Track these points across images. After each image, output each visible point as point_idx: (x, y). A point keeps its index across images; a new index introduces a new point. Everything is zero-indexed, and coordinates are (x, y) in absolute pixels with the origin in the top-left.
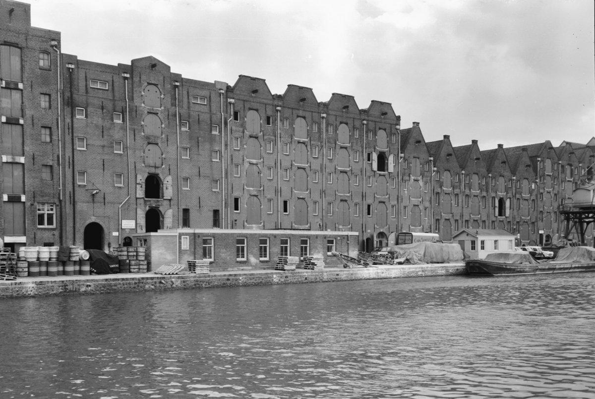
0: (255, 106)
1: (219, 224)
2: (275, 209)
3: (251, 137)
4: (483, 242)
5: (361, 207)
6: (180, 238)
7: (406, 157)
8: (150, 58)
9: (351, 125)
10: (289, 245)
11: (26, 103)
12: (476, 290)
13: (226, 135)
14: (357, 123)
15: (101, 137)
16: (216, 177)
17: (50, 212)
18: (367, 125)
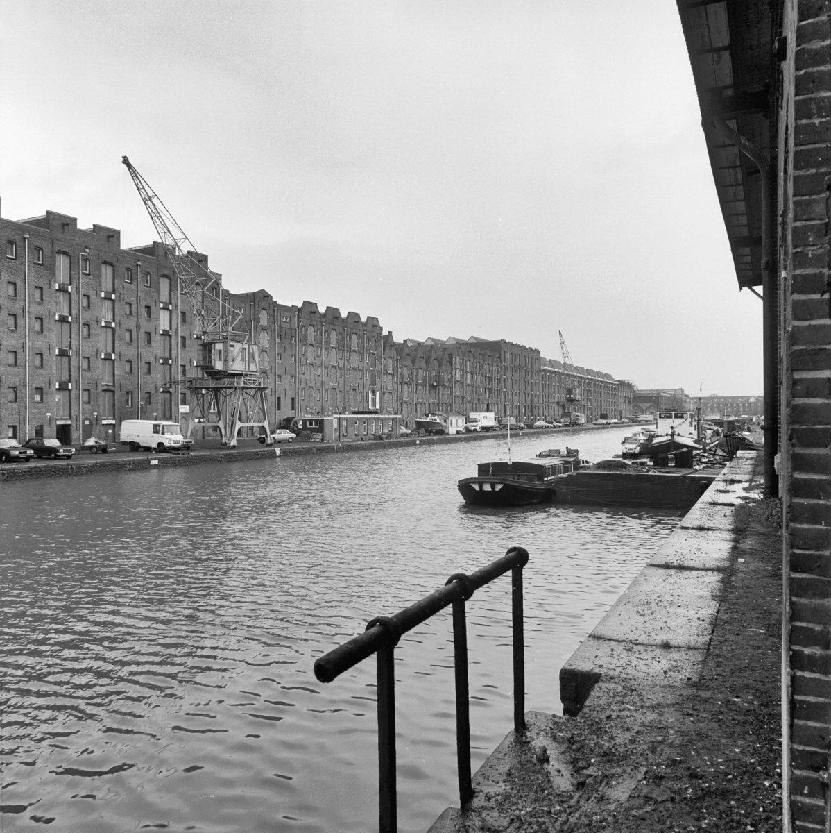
8: (262, 291)
16: (294, 373)
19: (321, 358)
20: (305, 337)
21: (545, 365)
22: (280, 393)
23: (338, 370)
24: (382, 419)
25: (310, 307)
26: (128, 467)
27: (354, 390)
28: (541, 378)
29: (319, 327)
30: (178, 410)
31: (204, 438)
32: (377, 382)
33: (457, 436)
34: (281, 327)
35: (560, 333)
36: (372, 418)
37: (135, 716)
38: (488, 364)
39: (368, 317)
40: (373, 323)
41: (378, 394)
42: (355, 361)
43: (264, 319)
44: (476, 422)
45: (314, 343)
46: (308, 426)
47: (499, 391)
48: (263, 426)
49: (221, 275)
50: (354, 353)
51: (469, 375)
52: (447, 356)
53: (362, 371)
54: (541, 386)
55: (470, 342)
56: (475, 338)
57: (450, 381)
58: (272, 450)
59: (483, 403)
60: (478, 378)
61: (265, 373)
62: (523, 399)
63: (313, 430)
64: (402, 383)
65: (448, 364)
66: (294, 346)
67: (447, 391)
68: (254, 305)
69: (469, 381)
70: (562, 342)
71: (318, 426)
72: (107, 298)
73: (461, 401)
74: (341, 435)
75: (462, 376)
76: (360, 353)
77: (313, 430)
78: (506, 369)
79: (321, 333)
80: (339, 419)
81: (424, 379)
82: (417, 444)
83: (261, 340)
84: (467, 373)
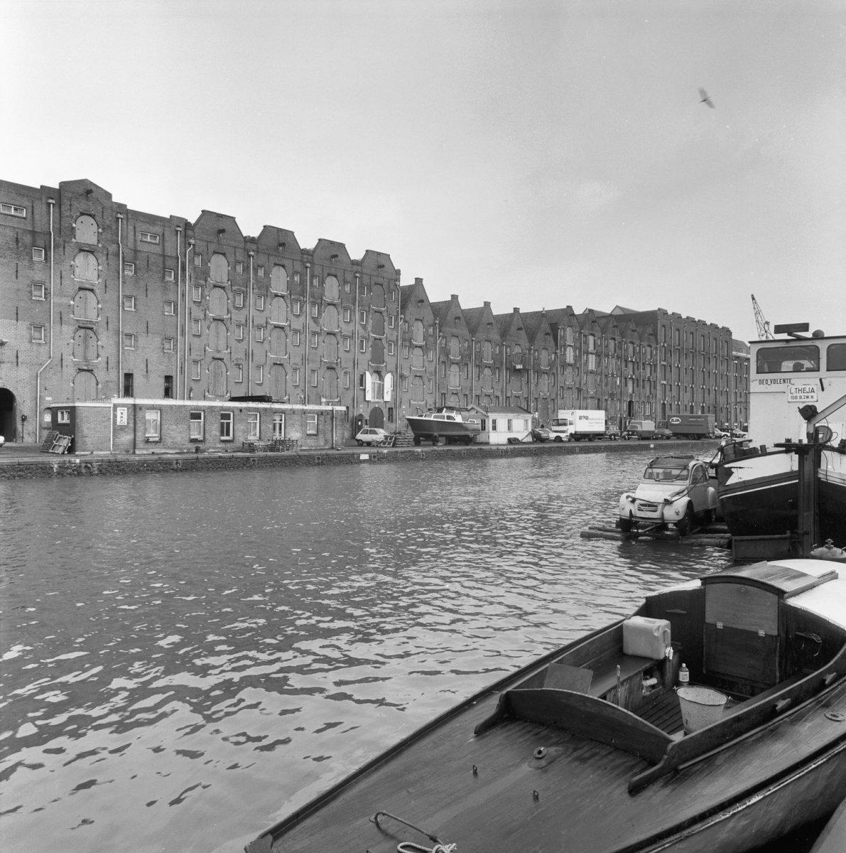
0: (333, 271)
2: (245, 376)
4: (494, 422)
7: (408, 319)
9: (341, 278)
10: (232, 420)
13: (184, 281)
14: (349, 277)
15: (14, 277)
16: (170, 333)
20: (205, 274)
21: (740, 350)
24: (283, 412)
28: (732, 368)
29: (240, 257)
32: (386, 358)
34: (136, 251)
35: (753, 299)
36: (249, 409)
37: (293, 711)
38: (650, 346)
39: (367, 251)
41: (388, 379)
42: (331, 319)
43: (87, 232)
44: (565, 425)
45: (227, 284)
47: (653, 385)
53: (352, 337)
54: (733, 379)
55: (615, 313)
57: (551, 364)
59: (620, 400)
60: (612, 364)
61: (91, 329)
62: (699, 397)
64: (446, 362)
65: (550, 338)
66: (172, 287)
67: (545, 380)
73: (575, 395)
76: (346, 309)
78: (668, 351)
80: (135, 408)
81: (497, 359)
82: (651, 449)
83: (77, 271)
84: (588, 353)
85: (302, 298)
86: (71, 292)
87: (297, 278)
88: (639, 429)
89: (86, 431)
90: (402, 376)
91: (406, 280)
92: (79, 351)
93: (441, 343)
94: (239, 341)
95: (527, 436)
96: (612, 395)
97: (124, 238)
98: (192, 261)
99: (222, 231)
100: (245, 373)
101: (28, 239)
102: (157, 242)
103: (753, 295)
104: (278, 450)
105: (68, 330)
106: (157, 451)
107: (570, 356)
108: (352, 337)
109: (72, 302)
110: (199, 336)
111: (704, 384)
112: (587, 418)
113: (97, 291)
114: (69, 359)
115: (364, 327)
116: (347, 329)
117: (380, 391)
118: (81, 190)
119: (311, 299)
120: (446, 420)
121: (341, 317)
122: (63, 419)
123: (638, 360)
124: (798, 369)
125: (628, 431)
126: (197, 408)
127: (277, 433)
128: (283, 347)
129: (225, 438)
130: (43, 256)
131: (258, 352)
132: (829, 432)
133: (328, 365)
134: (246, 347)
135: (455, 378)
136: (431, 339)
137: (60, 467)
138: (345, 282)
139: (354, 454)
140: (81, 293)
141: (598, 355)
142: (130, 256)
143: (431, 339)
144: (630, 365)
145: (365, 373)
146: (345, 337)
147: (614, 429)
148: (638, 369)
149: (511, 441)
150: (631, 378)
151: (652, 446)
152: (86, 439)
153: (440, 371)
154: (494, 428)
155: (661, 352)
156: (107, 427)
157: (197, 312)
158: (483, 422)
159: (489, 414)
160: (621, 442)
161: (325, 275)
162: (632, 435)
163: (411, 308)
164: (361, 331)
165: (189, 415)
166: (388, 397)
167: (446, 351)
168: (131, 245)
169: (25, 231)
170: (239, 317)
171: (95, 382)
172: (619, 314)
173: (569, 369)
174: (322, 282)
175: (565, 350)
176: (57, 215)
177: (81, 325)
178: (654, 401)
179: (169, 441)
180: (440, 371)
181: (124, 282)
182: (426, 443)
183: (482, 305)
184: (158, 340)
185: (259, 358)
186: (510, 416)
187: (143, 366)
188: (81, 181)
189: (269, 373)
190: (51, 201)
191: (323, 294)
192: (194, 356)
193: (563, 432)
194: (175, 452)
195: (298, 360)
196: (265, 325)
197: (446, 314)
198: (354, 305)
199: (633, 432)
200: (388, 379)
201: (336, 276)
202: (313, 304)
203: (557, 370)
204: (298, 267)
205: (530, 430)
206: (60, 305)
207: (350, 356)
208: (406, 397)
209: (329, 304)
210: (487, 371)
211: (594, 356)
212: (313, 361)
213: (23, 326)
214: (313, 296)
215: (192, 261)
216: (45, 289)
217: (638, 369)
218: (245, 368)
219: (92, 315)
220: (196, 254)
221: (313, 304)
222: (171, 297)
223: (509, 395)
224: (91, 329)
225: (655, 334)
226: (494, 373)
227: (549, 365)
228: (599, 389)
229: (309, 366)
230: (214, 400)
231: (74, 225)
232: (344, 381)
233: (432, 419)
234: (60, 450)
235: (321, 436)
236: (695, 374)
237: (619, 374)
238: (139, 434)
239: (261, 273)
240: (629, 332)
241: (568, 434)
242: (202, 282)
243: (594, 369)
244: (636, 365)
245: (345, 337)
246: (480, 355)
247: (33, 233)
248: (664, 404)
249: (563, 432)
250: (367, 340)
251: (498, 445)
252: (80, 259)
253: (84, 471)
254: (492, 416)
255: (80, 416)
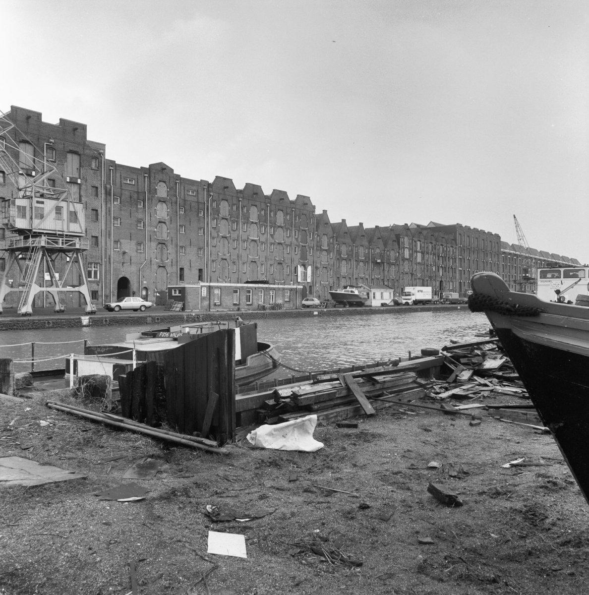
0: (281, 208)
1: (202, 279)
2: (237, 268)
3: (223, 219)
4: (374, 294)
5: (291, 268)
6: (201, 289)
7: (319, 234)
8: (161, 164)
9: (285, 211)
10: (238, 294)
11: (82, 193)
12: (294, 343)
13: (208, 216)
14: (289, 211)
15: (129, 217)
16: (201, 245)
17: (96, 269)
18: (270, 206)
19: (265, 235)
20: (217, 211)
22: (184, 263)
23: (259, 244)
24: (274, 289)
25: (223, 185)
26: (48, 326)
27: (280, 264)
28: (501, 260)
29: (235, 202)
30: (43, 277)
31: (80, 306)
33: (382, 308)
34: (185, 200)
35: (515, 217)
36: (259, 288)
38: (452, 247)
39: (298, 195)
40: (304, 202)
41: (309, 269)
42: (280, 235)
43: (162, 191)
44: (410, 295)
46: (173, 294)
48: (80, 292)
49: (104, 145)
50: (280, 229)
51: (419, 255)
52: (394, 236)
54: (501, 266)
56: (434, 223)
57: (397, 259)
58: (77, 319)
60: (430, 258)
61: (164, 244)
63: (176, 298)
64: (340, 259)
65: (396, 244)
67: (393, 268)
68: (149, 177)
69: (419, 260)
70: (517, 226)
71: (180, 295)
72: (73, 182)
74: (212, 304)
75: (411, 255)
76: (287, 229)
77: (176, 298)
78: (463, 250)
79: (238, 208)
80: (210, 288)
83: (158, 212)
84: (417, 252)
85: (265, 223)
86: (155, 223)
87: (263, 212)
88: (450, 297)
89: (189, 300)
90: (317, 268)
91: (318, 211)
92: (159, 256)
93: (337, 248)
94: (234, 249)
95: (391, 302)
96: (430, 277)
97: (180, 193)
98: (212, 205)
99: (227, 187)
100: (237, 266)
101: (135, 196)
102: (195, 195)
103: (514, 215)
104: (275, 310)
105: (154, 244)
106: (219, 310)
107: (407, 254)
108: (291, 245)
109: (156, 230)
110: (215, 246)
111: (478, 269)
112: (422, 291)
113: (167, 223)
114: (155, 261)
115: (297, 239)
116: (288, 241)
117: (305, 275)
118: (159, 168)
119: (270, 224)
120: (350, 293)
121: (285, 234)
122: (175, 293)
123: (445, 256)
124: (553, 277)
125: (444, 299)
126: (236, 287)
127: (271, 301)
128: (256, 252)
129: (248, 303)
130: (142, 205)
131: (244, 254)
132: (564, 298)
133: (278, 262)
134: (266, 255)
135: (344, 269)
136: (331, 245)
137: (187, 317)
138: (287, 214)
139: (311, 311)
140: (160, 224)
141: (423, 253)
142: (182, 204)
143: (331, 245)
144: (441, 259)
145: (297, 266)
146: (287, 246)
147: (436, 298)
148: (445, 260)
149: (383, 305)
150: (442, 267)
151: (459, 308)
152: (189, 304)
153: (336, 264)
154: (374, 297)
155: (458, 250)
156: (198, 297)
157: (215, 234)
158: (368, 294)
159: (371, 290)
160: (440, 306)
161: (277, 210)
162: (446, 301)
163: (321, 228)
164: (295, 242)
165: (232, 291)
166: (309, 280)
167: (339, 253)
168: (182, 197)
169: (135, 192)
170: (234, 235)
171: (166, 273)
172: (433, 226)
173: (406, 262)
174: (275, 214)
175: (404, 250)
176: (149, 183)
177: (160, 242)
178: (455, 280)
179: (224, 304)
180: (336, 264)
181: (180, 218)
182: (339, 306)
183: (341, 221)
184: (195, 249)
185: (244, 259)
186: (382, 290)
187: (188, 264)
188: (159, 163)
189: (249, 267)
190: (146, 175)
191: (275, 222)
192: (213, 258)
193: (409, 299)
194: (227, 310)
195: (264, 259)
196: (237, 238)
197: (341, 232)
198: (292, 227)
199: (447, 299)
200: (309, 269)
201: (282, 211)
202: (271, 227)
203: (400, 262)
204: (263, 206)
205: (392, 298)
206: (151, 231)
207: (289, 256)
208: (318, 280)
209: (279, 227)
210: (361, 264)
211: (420, 253)
212: (271, 260)
213: (134, 243)
214: (270, 223)
215: (212, 205)
216: (143, 223)
217: (445, 260)
218: (237, 263)
219: (165, 236)
220: (213, 201)
221: (271, 227)
222: (202, 225)
223: (373, 277)
224: (164, 244)
225: (455, 240)
226: (365, 265)
227: (395, 260)
228: (423, 274)
229: (269, 263)
230: (222, 282)
231: (156, 188)
232: (287, 271)
233: (343, 292)
234: (178, 309)
235: (291, 302)
236: (479, 263)
237: (434, 263)
238: (212, 301)
239: (245, 210)
240: (440, 238)
241: (412, 301)
242: (217, 216)
243: (420, 261)
244: (444, 258)
245: (287, 246)
246: (357, 254)
247: (138, 193)
248: (460, 282)
249: (409, 299)
250: (298, 246)
251: (376, 307)
252: (159, 206)
253: (196, 319)
254: (373, 290)
255: (187, 291)
